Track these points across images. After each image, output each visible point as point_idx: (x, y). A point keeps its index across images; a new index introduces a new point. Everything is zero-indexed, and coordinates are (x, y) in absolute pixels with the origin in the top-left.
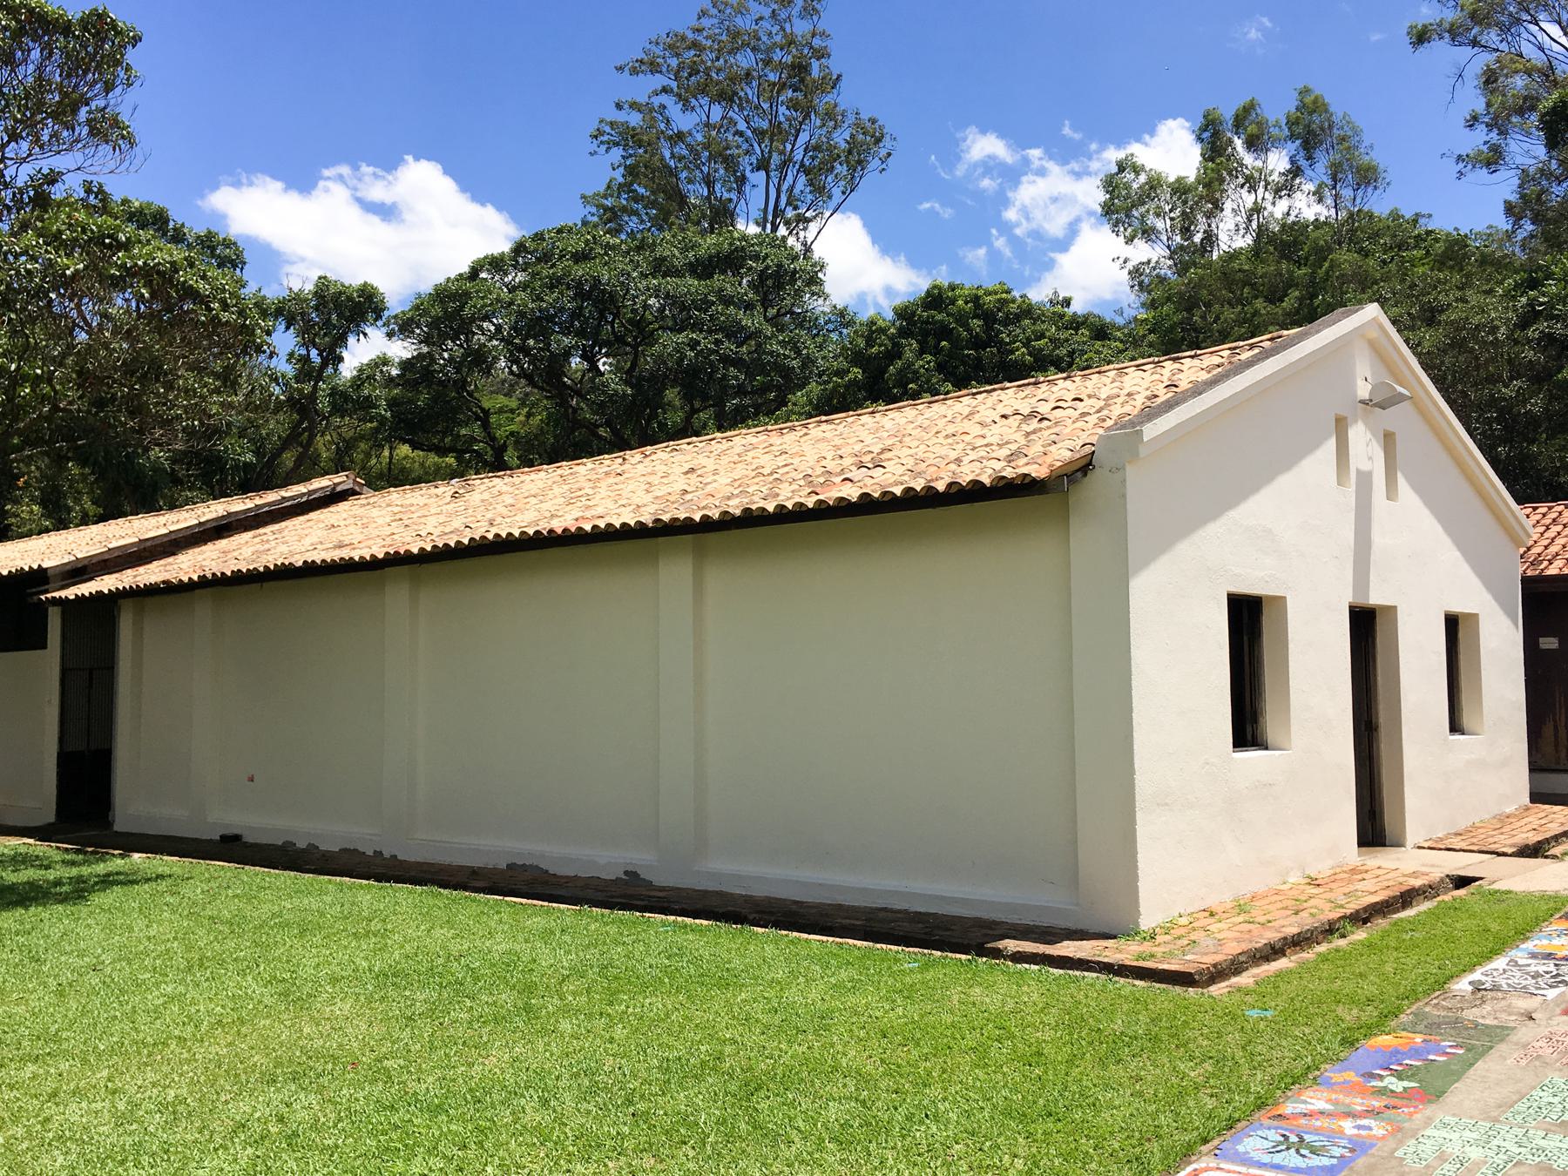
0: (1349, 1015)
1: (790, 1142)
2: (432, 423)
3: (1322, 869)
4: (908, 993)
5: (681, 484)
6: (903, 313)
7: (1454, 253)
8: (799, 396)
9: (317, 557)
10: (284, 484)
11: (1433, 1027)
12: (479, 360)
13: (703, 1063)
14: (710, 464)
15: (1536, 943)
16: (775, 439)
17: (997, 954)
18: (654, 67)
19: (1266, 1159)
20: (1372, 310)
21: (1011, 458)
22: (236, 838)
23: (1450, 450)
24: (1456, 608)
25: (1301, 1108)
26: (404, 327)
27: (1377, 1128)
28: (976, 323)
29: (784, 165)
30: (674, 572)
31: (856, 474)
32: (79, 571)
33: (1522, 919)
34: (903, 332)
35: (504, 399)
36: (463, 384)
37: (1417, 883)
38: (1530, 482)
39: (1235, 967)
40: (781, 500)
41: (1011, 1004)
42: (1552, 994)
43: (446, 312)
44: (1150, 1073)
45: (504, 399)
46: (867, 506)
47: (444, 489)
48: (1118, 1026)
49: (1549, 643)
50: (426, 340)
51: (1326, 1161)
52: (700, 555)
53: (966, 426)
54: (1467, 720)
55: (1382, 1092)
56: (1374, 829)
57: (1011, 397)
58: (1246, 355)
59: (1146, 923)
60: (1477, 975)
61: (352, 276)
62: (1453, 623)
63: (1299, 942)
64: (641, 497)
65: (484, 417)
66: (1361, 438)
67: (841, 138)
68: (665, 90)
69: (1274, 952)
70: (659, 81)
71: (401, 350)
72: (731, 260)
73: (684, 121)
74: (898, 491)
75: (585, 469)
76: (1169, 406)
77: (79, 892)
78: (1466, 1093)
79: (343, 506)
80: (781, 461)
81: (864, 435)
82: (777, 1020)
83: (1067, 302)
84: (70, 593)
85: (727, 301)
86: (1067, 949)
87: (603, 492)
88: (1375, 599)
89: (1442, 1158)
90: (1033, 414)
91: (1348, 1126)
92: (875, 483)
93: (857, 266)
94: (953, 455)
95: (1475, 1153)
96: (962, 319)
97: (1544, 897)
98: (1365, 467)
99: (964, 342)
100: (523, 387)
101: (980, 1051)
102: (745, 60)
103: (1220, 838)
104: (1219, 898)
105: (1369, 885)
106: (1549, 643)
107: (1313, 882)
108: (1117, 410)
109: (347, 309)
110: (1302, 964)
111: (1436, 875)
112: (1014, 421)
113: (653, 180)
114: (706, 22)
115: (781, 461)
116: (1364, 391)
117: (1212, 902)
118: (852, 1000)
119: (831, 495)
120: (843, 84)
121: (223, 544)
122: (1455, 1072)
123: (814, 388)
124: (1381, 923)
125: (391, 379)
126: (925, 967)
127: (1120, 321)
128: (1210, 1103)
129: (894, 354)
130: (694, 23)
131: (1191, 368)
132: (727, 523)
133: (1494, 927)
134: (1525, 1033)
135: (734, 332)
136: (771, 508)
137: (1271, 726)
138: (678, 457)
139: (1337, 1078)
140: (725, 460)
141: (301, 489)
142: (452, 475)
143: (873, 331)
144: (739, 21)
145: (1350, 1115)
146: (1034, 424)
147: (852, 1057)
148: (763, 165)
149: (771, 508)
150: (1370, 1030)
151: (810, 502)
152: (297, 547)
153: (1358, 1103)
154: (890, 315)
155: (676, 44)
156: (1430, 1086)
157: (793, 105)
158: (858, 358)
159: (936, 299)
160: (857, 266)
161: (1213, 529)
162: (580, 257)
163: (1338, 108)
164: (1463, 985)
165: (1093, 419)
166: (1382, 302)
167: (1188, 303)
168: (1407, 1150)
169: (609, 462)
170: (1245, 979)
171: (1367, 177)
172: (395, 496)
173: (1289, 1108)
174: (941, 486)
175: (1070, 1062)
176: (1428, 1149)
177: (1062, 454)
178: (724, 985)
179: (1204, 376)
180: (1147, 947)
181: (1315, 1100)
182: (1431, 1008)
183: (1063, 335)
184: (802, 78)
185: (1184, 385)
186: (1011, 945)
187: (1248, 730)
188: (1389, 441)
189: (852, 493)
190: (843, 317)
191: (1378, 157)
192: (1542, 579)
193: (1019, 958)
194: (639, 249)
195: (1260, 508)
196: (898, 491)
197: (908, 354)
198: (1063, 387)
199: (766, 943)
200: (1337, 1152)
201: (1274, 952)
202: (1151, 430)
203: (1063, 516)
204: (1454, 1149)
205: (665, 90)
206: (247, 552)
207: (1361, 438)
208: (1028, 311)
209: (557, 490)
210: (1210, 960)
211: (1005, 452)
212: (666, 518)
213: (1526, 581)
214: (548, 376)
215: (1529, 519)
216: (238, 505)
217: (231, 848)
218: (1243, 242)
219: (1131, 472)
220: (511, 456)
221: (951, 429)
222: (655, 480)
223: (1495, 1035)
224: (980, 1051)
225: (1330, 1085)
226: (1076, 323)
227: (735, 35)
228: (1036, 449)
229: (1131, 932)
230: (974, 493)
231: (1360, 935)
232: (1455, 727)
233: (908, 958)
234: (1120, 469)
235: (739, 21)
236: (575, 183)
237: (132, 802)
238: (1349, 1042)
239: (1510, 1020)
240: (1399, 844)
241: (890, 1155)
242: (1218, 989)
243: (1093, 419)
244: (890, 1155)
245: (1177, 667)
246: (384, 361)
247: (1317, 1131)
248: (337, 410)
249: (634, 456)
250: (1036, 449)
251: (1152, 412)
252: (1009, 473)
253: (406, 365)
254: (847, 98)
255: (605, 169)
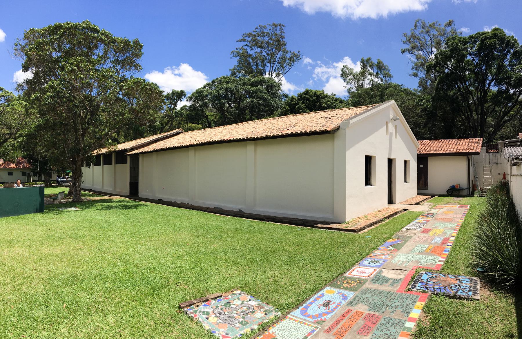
0: (384, 236)
1: (275, 265)
2: (196, 118)
3: (381, 208)
4: (298, 235)
5: (251, 130)
6: (300, 95)
7: (407, 92)
8: (276, 112)
9: (176, 145)
10: (168, 131)
11: (399, 237)
12: (206, 105)
13: (257, 249)
14: (258, 126)
15: (416, 221)
16: (272, 121)
17: (317, 227)
18: (244, 40)
19: (368, 265)
20: (393, 102)
21: (323, 126)
22: (161, 200)
23: (406, 130)
24: (406, 159)
25: (375, 254)
26: (190, 99)
27: (389, 257)
28: (315, 98)
29: (274, 61)
30: (250, 148)
31: (290, 128)
32: (132, 149)
33: (415, 216)
34: (299, 99)
35: (210, 112)
36: (203, 110)
37: (398, 211)
38: (420, 137)
39: (364, 228)
40: (274, 134)
41: (319, 237)
42: (419, 229)
43: (198, 95)
44: (347, 250)
45: (210, 112)
46: (292, 135)
47: (200, 131)
48: (341, 241)
49: (422, 166)
50: (194, 101)
51: (379, 264)
52: (256, 145)
53: (314, 119)
54: (407, 180)
55: (389, 250)
56: (390, 201)
57: (323, 114)
58: (370, 108)
59: (348, 219)
60: (407, 227)
61: (179, 89)
62: (406, 162)
63: (376, 223)
64: (243, 133)
65: (207, 117)
66: (391, 126)
67: (289, 56)
68: (247, 45)
69: (371, 225)
70: (245, 43)
71: (189, 104)
72: (261, 83)
73: (251, 52)
74: (299, 132)
75: (230, 127)
76: (355, 117)
77: (136, 207)
78: (404, 249)
79: (180, 135)
80: (273, 126)
81: (291, 120)
82: (272, 240)
83: (335, 95)
84: (131, 153)
85: (261, 92)
86: (331, 226)
87: (234, 131)
88: (392, 157)
89: (399, 261)
90: (327, 117)
91: (383, 257)
92: (294, 130)
93: (288, 87)
94: (311, 125)
95: (405, 260)
96: (312, 97)
97: (419, 212)
98: (391, 132)
99: (313, 102)
100: (215, 110)
101: (313, 247)
102: (266, 39)
103: (362, 204)
104: (361, 215)
105: (389, 211)
106: (422, 166)
107: (379, 211)
108: (345, 117)
109: (179, 95)
110: (377, 227)
111: (401, 209)
112: (323, 119)
113: (245, 63)
114: (257, 30)
115: (273, 126)
116: (391, 117)
117: (360, 216)
118: (287, 236)
119: (284, 133)
120: (287, 45)
121: (157, 143)
122: (402, 245)
123: (279, 111)
124: (391, 218)
125: (187, 110)
126: (302, 230)
127: (345, 100)
128: (358, 255)
129: (297, 104)
130: (254, 30)
131: (359, 110)
132: (262, 138)
133: (410, 218)
134: (414, 237)
135: (262, 98)
136: (272, 135)
137: (372, 181)
138: (250, 125)
139: (382, 248)
140: (261, 125)
141: (171, 132)
142: (200, 129)
143: (292, 99)
144: (265, 30)
145: (384, 255)
146: (328, 119)
147: (287, 248)
148: (269, 62)
149: (272, 135)
150: (388, 238)
151: (280, 134)
152: (172, 144)
153: (385, 253)
154: (296, 96)
155: (249, 35)
156: (398, 248)
157: (276, 49)
158: (289, 105)
159: (307, 92)
160: (288, 87)
161: (363, 142)
162: (227, 83)
163: (385, 63)
164: (404, 229)
165: (340, 119)
166: (396, 100)
167: (359, 96)
168: (393, 261)
169: (235, 126)
170: (366, 230)
171: (390, 76)
172: (190, 133)
173: (372, 255)
174: (308, 132)
175: (331, 248)
176: (397, 260)
177: (333, 126)
178: (260, 233)
179: (362, 112)
180: (347, 225)
181: (377, 252)
182: (399, 234)
183: (333, 102)
184: (279, 43)
185: (358, 113)
186: (320, 225)
187: (368, 182)
188: (396, 127)
189: (289, 132)
190: (286, 96)
191: (391, 73)
192: (421, 154)
193: (321, 228)
194: (240, 80)
195: (371, 139)
196: (299, 132)
197: (300, 104)
198: (333, 112)
199: (269, 225)
200: (381, 262)
201: (371, 225)
202: (351, 122)
203: (333, 139)
204: (401, 260)
205: (247, 45)
206: (162, 145)
207: (391, 126)
208: (326, 96)
209: (224, 131)
210: (359, 227)
211: (322, 125)
212: (249, 137)
213: (418, 154)
214: (220, 108)
215: (419, 143)
216: (160, 136)
217: (160, 201)
218: (369, 86)
219: (347, 130)
220: (213, 124)
221: (310, 120)
222: (246, 129)
223: (409, 237)
224: (313, 247)
225: (381, 250)
226: (336, 100)
227: (263, 33)
228: (328, 125)
229: (344, 222)
230: (315, 133)
231: (387, 221)
232: (405, 182)
233: (298, 228)
234: (345, 129)
235: (265, 30)
236: (226, 67)
237: (143, 192)
238: (384, 241)
239: (412, 235)
240: (395, 203)
241: (295, 267)
242: (360, 233)
243: (340, 119)
244: (295, 267)
245: (355, 170)
246: (186, 106)
247: (377, 259)
248: (176, 116)
249: (241, 124)
250: (328, 125)
251: (351, 118)
252: (322, 129)
253: (190, 107)
254: (288, 48)
255: (234, 62)
